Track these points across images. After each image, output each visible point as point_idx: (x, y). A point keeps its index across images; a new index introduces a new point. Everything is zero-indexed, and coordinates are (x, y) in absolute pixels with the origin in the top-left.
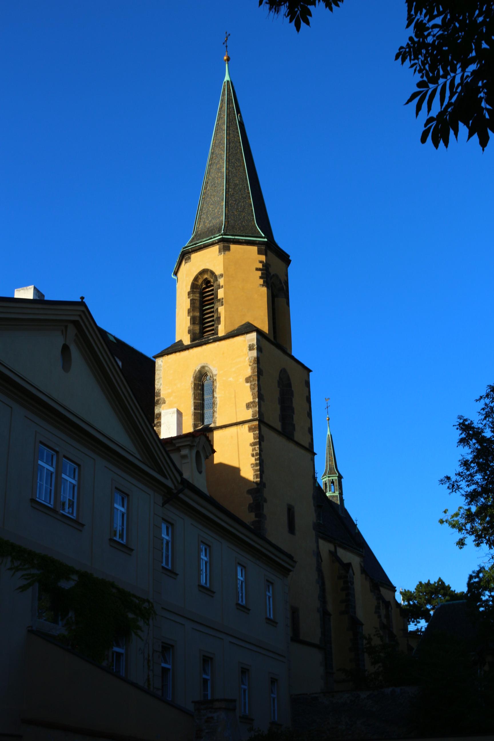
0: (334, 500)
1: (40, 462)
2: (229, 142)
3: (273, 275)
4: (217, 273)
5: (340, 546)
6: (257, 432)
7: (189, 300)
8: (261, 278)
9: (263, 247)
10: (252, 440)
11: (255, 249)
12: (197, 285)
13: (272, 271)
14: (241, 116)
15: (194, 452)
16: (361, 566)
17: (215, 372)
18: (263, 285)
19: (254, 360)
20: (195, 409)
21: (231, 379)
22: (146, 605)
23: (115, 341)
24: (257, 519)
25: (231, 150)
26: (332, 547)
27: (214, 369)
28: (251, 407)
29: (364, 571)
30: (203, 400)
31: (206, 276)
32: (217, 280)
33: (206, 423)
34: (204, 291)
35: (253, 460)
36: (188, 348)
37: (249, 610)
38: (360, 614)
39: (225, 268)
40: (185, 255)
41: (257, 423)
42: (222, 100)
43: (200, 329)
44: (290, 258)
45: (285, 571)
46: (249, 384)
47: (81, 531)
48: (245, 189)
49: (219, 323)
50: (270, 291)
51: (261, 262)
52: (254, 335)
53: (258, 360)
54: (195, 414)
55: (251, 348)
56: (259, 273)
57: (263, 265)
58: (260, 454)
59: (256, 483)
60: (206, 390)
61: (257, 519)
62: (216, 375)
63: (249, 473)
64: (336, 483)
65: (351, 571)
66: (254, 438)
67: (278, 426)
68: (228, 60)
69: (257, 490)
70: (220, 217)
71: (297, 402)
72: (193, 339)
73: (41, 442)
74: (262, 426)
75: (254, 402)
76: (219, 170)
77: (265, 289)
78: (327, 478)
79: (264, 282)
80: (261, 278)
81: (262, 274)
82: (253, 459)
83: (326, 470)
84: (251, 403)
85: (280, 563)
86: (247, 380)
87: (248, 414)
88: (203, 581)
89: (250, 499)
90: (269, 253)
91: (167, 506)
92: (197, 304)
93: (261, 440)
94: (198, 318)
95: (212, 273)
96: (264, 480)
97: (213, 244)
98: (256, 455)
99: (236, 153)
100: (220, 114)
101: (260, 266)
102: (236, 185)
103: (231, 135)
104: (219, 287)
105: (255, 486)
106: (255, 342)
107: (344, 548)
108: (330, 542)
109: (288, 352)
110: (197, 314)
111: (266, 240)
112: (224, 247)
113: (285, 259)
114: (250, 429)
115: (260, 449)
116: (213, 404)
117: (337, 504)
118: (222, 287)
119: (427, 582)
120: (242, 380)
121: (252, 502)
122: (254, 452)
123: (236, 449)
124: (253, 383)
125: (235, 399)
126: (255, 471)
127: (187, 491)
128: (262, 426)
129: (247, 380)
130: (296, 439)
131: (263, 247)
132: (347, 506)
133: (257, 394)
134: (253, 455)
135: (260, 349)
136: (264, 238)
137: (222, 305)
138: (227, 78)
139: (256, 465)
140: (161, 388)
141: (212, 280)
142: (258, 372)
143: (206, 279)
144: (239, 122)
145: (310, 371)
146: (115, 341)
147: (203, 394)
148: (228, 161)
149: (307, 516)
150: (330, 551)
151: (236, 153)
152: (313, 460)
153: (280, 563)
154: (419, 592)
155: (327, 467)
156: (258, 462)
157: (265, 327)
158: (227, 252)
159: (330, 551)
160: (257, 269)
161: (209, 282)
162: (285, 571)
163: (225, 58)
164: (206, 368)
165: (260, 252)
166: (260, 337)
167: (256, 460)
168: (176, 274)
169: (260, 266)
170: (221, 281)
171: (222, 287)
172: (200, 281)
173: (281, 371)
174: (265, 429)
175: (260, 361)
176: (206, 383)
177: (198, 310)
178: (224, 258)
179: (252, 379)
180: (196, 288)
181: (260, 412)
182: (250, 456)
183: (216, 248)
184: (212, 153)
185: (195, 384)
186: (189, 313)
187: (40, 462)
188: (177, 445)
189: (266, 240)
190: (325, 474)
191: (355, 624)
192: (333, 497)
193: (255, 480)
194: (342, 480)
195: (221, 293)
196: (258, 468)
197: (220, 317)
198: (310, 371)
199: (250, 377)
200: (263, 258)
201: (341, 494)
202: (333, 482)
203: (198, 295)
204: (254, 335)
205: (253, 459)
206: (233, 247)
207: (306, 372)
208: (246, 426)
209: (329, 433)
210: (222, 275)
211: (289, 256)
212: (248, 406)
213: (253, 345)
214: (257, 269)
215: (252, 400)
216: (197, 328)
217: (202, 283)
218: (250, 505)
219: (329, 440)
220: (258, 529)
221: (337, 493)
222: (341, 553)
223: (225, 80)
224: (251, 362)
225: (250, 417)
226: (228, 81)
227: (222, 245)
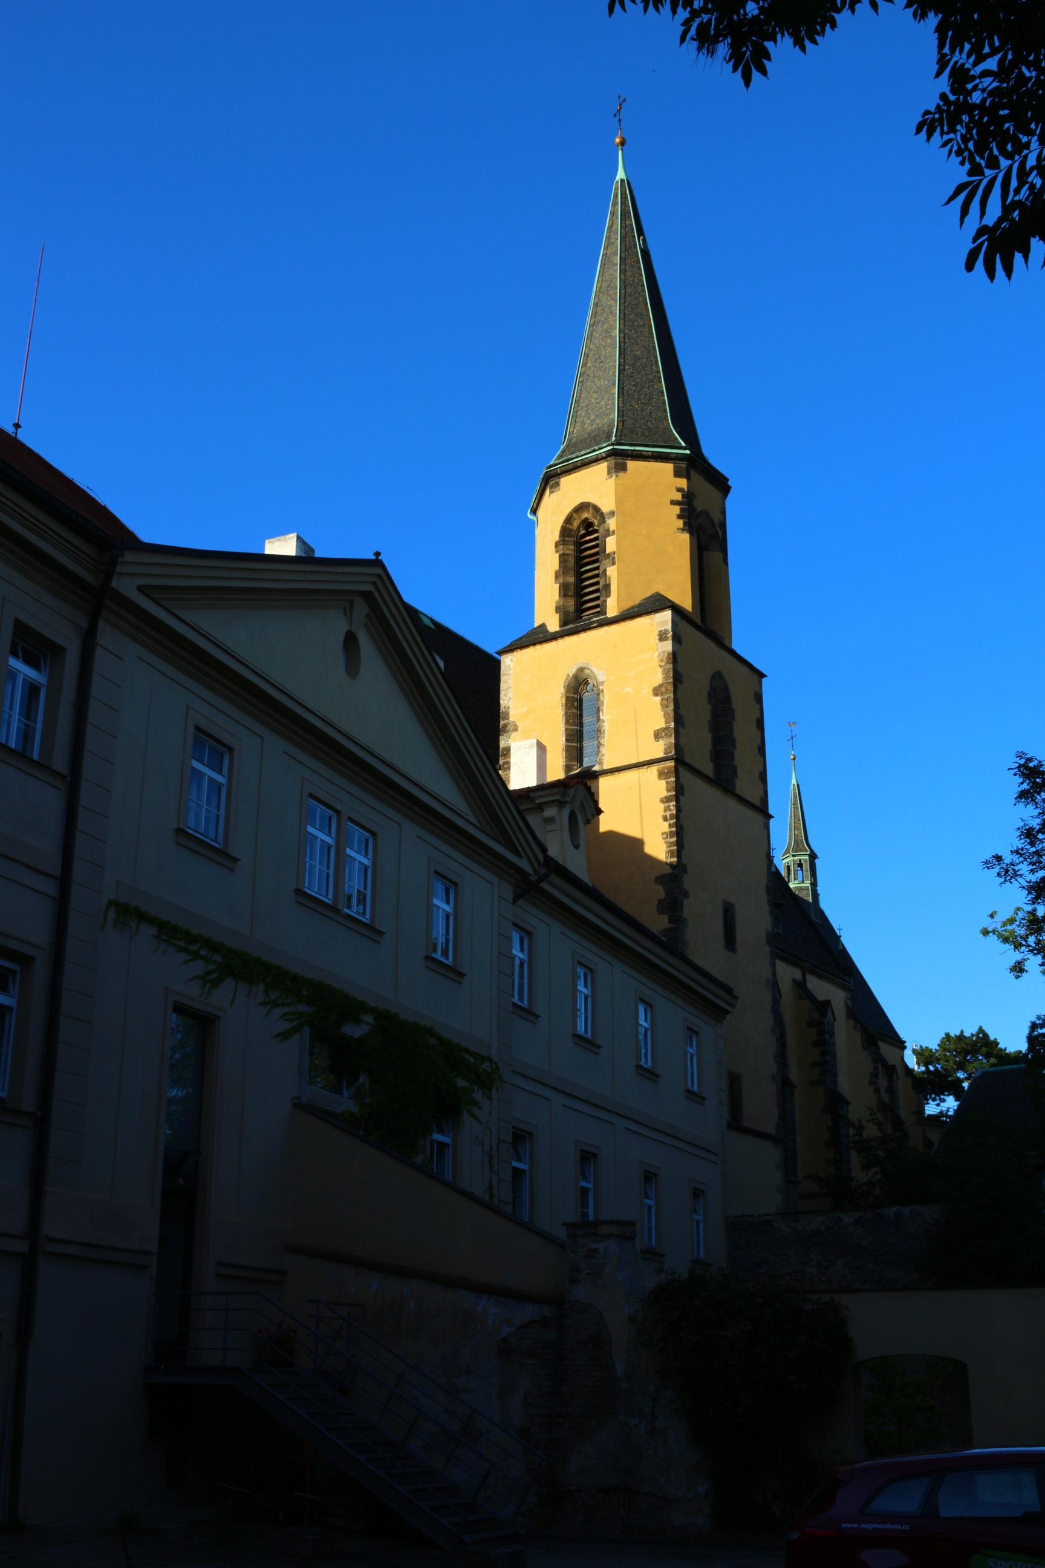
0: (802, 895)
1: (310, 829)
2: (624, 285)
3: (701, 512)
4: (605, 509)
5: (812, 973)
6: (673, 779)
7: (557, 556)
8: (679, 517)
9: (683, 465)
10: (665, 794)
11: (669, 467)
12: (571, 530)
13: (699, 505)
14: (644, 240)
15: (566, 813)
16: (847, 1007)
17: (600, 678)
18: (683, 530)
19: (668, 658)
20: (567, 740)
21: (628, 690)
22: (486, 1065)
23: (432, 626)
24: (672, 925)
25: (629, 299)
26: (797, 974)
27: (599, 673)
28: (662, 737)
29: (851, 1014)
30: (581, 725)
31: (585, 515)
32: (604, 522)
33: (585, 765)
34: (583, 540)
35: (665, 827)
36: (555, 637)
37: (658, 1076)
38: (845, 1085)
39: (619, 501)
40: (550, 480)
41: (672, 764)
42: (613, 214)
43: (576, 605)
44: (730, 483)
45: (718, 1013)
46: (658, 698)
47: (378, 942)
48: (651, 366)
49: (608, 595)
50: (695, 540)
51: (679, 490)
52: (667, 615)
53: (674, 658)
54: (568, 749)
55: (662, 637)
56: (677, 509)
57: (683, 496)
58: (677, 817)
59: (671, 865)
60: (587, 709)
61: (672, 925)
62: (603, 683)
63: (658, 847)
64: (807, 866)
65: (829, 1014)
66: (668, 790)
67: (709, 769)
68: (623, 143)
69: (672, 878)
70: (609, 414)
71: (741, 730)
72: (564, 623)
73: (312, 796)
74: (681, 769)
75: (667, 728)
76: (608, 333)
77: (686, 537)
78: (791, 858)
79: (684, 524)
80: (679, 517)
81: (681, 510)
82: (667, 824)
83: (790, 844)
84: (663, 729)
85: (710, 999)
86: (656, 691)
87: (658, 749)
88: (581, 1029)
89: (660, 892)
90: (693, 474)
91: (520, 902)
92: (571, 562)
93: (679, 792)
94: (572, 587)
95: (597, 509)
96: (684, 860)
97: (597, 460)
98: (671, 819)
99: (637, 305)
100: (608, 238)
101: (678, 497)
102: (636, 358)
103: (629, 273)
104: (608, 533)
105: (669, 870)
106: (669, 627)
107: (820, 976)
108: (795, 965)
109: (726, 643)
110: (571, 580)
111: (688, 452)
112: (616, 464)
113: (721, 484)
114: (661, 775)
115: (678, 808)
116: (598, 732)
117: (806, 902)
118: (613, 532)
119: (958, 1034)
120: (647, 691)
121: (663, 896)
122: (668, 814)
123: (637, 809)
124: (666, 696)
125: (636, 724)
126: (670, 844)
127: (554, 878)
128: (681, 769)
129: (656, 691)
130: (738, 791)
131: (683, 465)
132: (824, 904)
133: (672, 714)
134: (665, 819)
135: (677, 639)
136: (685, 448)
137: (614, 564)
138: (621, 174)
139: (671, 834)
140: (511, 704)
141: (596, 522)
142: (674, 677)
143: (586, 519)
144: (642, 251)
145: (764, 676)
146: (432, 626)
147: (581, 716)
148: (623, 317)
149: (756, 921)
150: (795, 981)
151: (637, 305)
152: (767, 827)
153: (710, 999)
154: (945, 1050)
155: (790, 839)
156: (674, 829)
157: (686, 602)
158: (621, 474)
159: (795, 981)
160: (673, 503)
161: (591, 524)
162: (718, 1013)
163: (618, 140)
164: (587, 671)
165: (677, 474)
166: (678, 619)
167: (670, 826)
168: (534, 512)
169: (678, 497)
170: (612, 523)
171: (613, 532)
172: (576, 524)
173: (713, 677)
174: (685, 775)
175: (679, 660)
176: (586, 696)
177: (572, 572)
178: (616, 484)
179: (663, 690)
180: (569, 536)
181: (677, 746)
182: (661, 819)
183: (603, 466)
184: (596, 305)
185: (567, 698)
186: (557, 577)
187: (310, 829)
188: (538, 801)
189: (688, 452)
190: (787, 852)
191: (836, 1102)
192: (801, 889)
193: (669, 861)
194: (817, 861)
195: (611, 544)
196: (675, 839)
197: (609, 585)
198: (764, 676)
199: (661, 686)
200: (683, 483)
201: (814, 884)
202: (800, 865)
203: (572, 547)
204: (667, 615)
205: (667, 824)
206: (631, 464)
207: (756, 676)
208: (654, 770)
209: (794, 781)
210: (612, 513)
211: (727, 480)
212: (657, 735)
213: (666, 632)
214: (673, 503)
215: (664, 726)
216: (571, 603)
217: (579, 528)
218: (660, 901)
219: (795, 797)
220: (673, 943)
221: (807, 884)
222: (821, 988)
223: (618, 178)
224: (662, 660)
225: (661, 755)
226: (622, 181)
227: (613, 461)
